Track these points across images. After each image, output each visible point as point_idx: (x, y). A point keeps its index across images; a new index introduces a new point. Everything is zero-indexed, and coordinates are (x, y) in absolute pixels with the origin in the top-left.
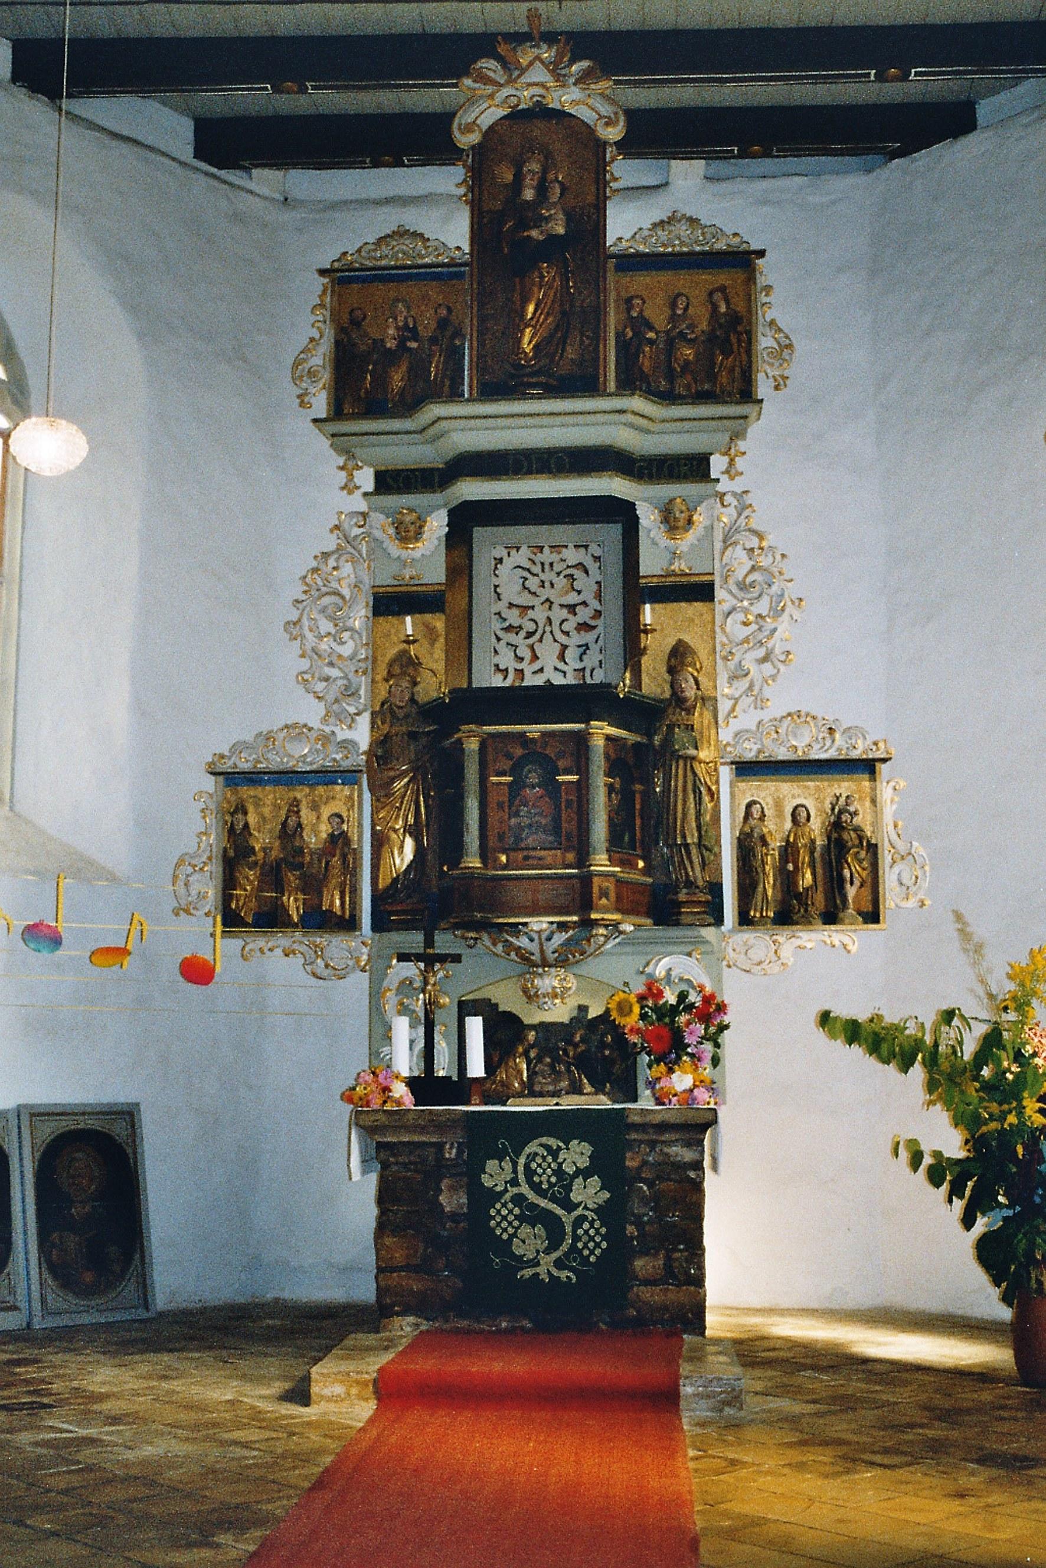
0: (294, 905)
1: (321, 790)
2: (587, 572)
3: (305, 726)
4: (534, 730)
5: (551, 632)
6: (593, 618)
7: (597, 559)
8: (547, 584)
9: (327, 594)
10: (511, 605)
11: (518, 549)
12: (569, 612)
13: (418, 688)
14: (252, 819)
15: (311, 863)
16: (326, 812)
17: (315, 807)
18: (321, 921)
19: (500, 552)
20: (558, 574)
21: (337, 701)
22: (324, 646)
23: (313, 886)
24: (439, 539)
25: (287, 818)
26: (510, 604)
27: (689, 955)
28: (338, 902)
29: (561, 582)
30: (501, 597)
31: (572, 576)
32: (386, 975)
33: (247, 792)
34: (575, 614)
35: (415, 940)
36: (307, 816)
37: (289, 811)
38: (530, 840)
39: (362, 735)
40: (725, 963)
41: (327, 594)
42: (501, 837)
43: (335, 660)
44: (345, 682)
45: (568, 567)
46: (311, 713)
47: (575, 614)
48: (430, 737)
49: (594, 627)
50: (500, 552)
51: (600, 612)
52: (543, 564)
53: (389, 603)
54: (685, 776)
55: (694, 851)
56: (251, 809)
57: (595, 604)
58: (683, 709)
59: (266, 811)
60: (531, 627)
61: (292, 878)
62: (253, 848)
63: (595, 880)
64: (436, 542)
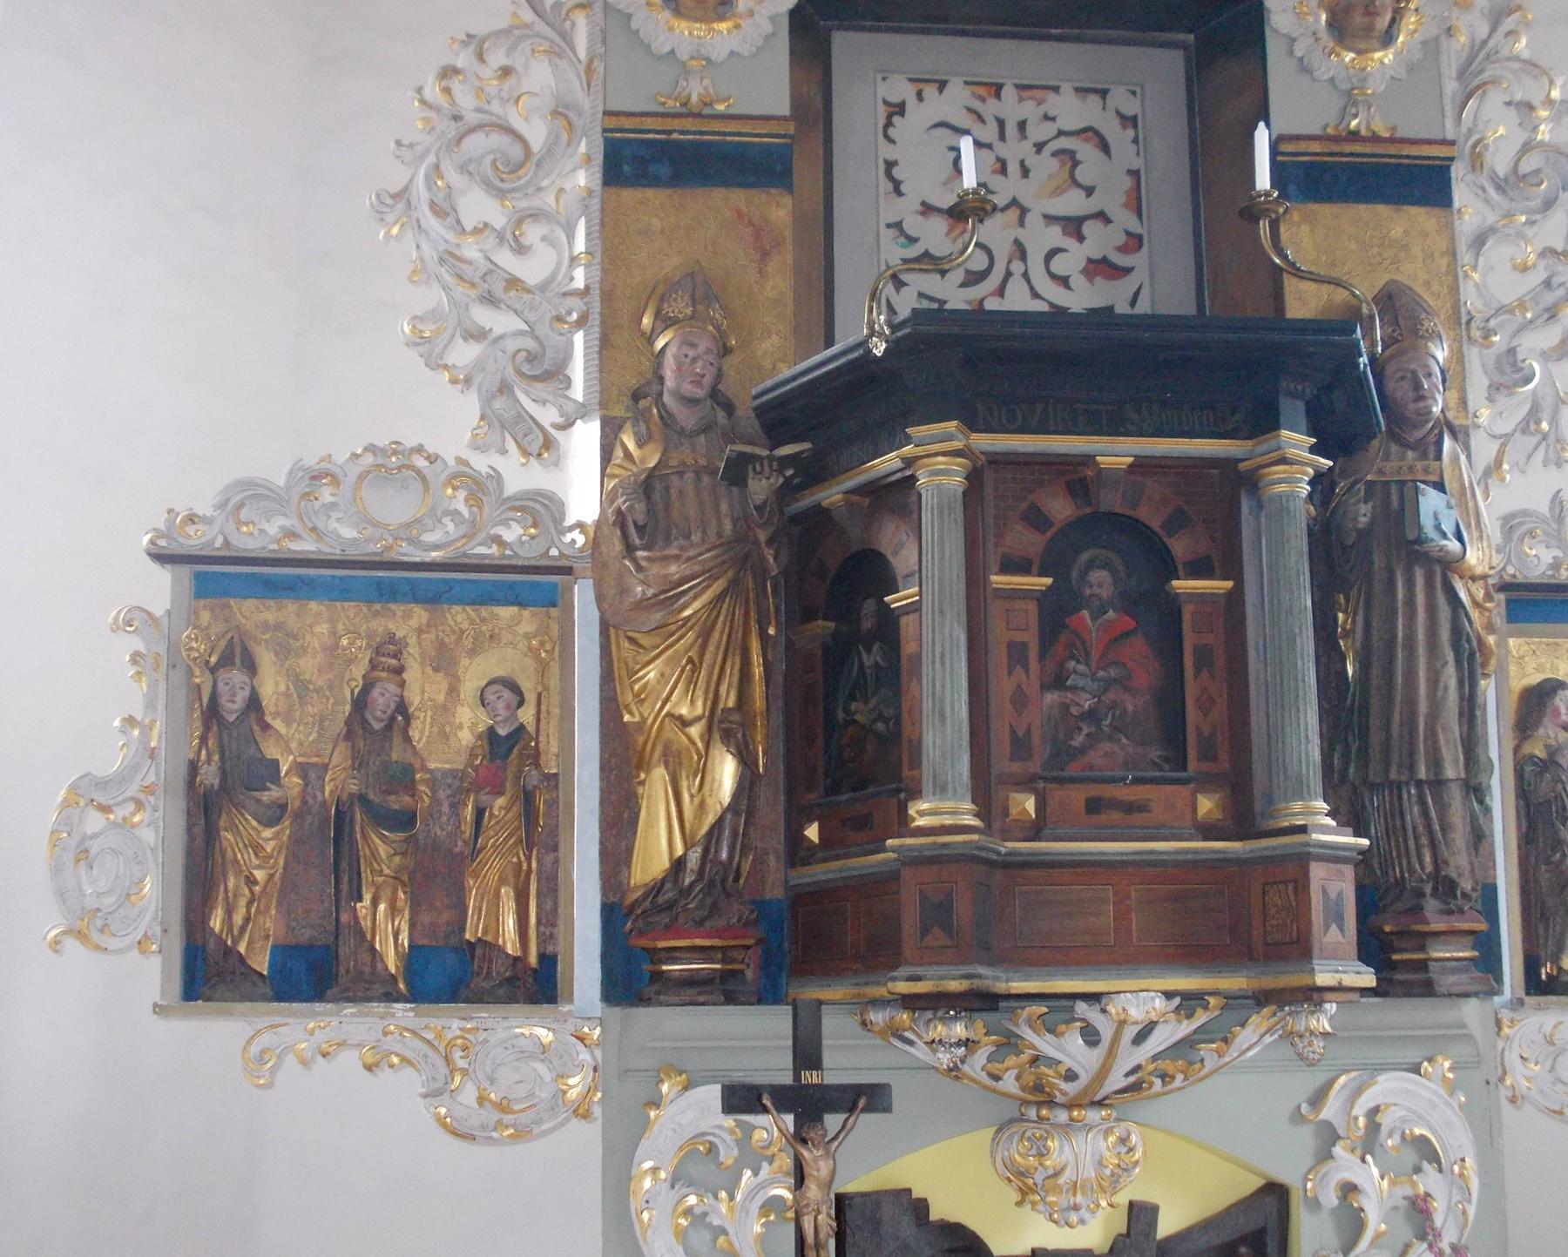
0: (390, 934)
1: (459, 616)
2: (1105, 147)
3: (419, 449)
4: (1115, 452)
5: (1026, 275)
6: (1124, 249)
7: (1129, 121)
8: (1013, 168)
9: (481, 127)
10: (927, 209)
11: (942, 85)
12: (1066, 233)
13: (730, 364)
14: (271, 686)
15: (431, 815)
16: (475, 673)
17: (443, 661)
18: (455, 973)
19: (900, 89)
20: (1039, 147)
21: (504, 388)
22: (471, 250)
23: (436, 877)
24: (772, 19)
25: (368, 687)
26: (923, 204)
27: (1416, 1069)
28: (510, 923)
29: (1046, 167)
30: (903, 188)
31: (1071, 154)
32: (646, 1124)
33: (252, 613)
34: (1081, 238)
35: (757, 1038)
36: (421, 686)
37: (374, 666)
38: (1095, 757)
39: (581, 485)
40: (1504, 1093)
41: (481, 127)
42: (1021, 747)
43: (498, 288)
44: (529, 344)
45: (1061, 133)
46: (447, 424)
47: (1081, 238)
48: (782, 515)
49: (1127, 271)
50: (900, 89)
51: (1139, 238)
52: (1001, 123)
53: (646, 158)
54: (1431, 609)
55: (1455, 796)
56: (266, 659)
57: (1125, 220)
58: (1406, 446)
59: (309, 666)
60: (980, 262)
61: (381, 850)
62: (275, 764)
63: (1317, 872)
64: (767, 27)
